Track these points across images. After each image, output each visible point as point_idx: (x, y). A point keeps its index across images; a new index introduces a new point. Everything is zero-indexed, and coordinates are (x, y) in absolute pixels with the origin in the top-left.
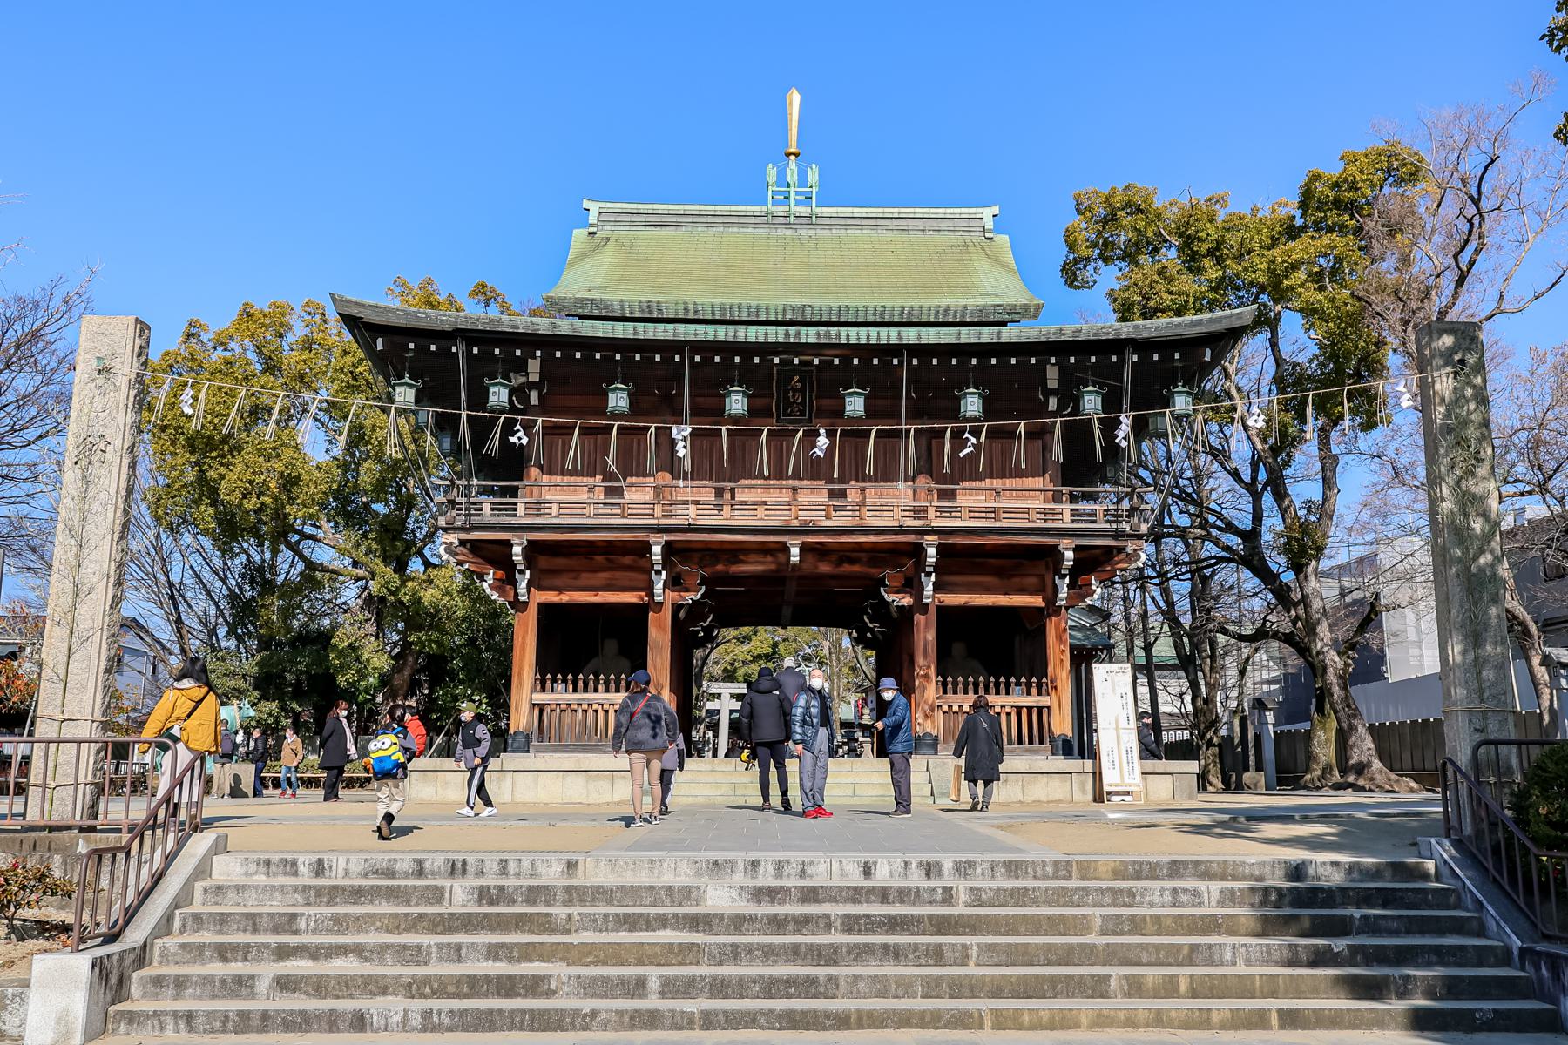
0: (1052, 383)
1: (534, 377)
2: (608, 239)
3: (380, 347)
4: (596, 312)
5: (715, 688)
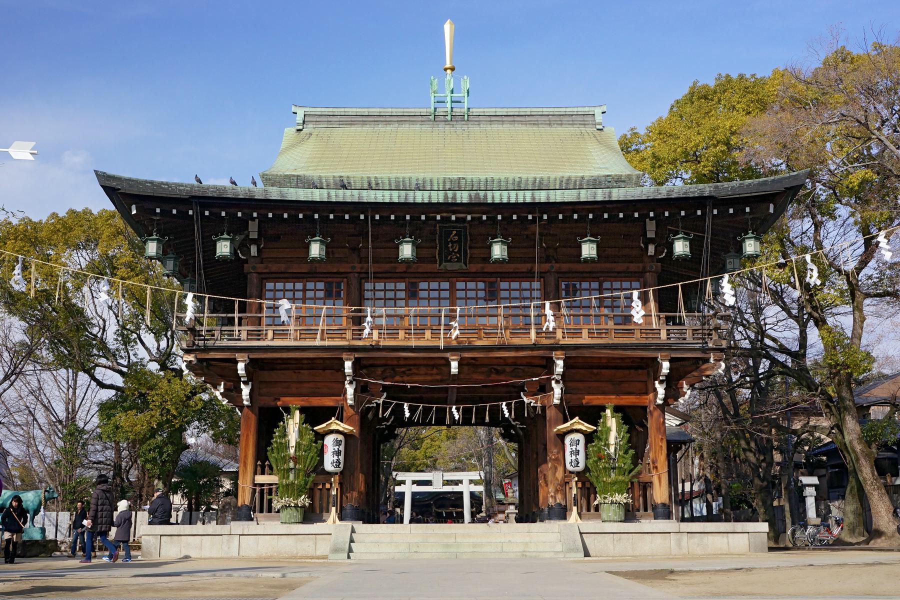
1: (254, 235)
2: (311, 134)
3: (134, 212)
5: (400, 476)
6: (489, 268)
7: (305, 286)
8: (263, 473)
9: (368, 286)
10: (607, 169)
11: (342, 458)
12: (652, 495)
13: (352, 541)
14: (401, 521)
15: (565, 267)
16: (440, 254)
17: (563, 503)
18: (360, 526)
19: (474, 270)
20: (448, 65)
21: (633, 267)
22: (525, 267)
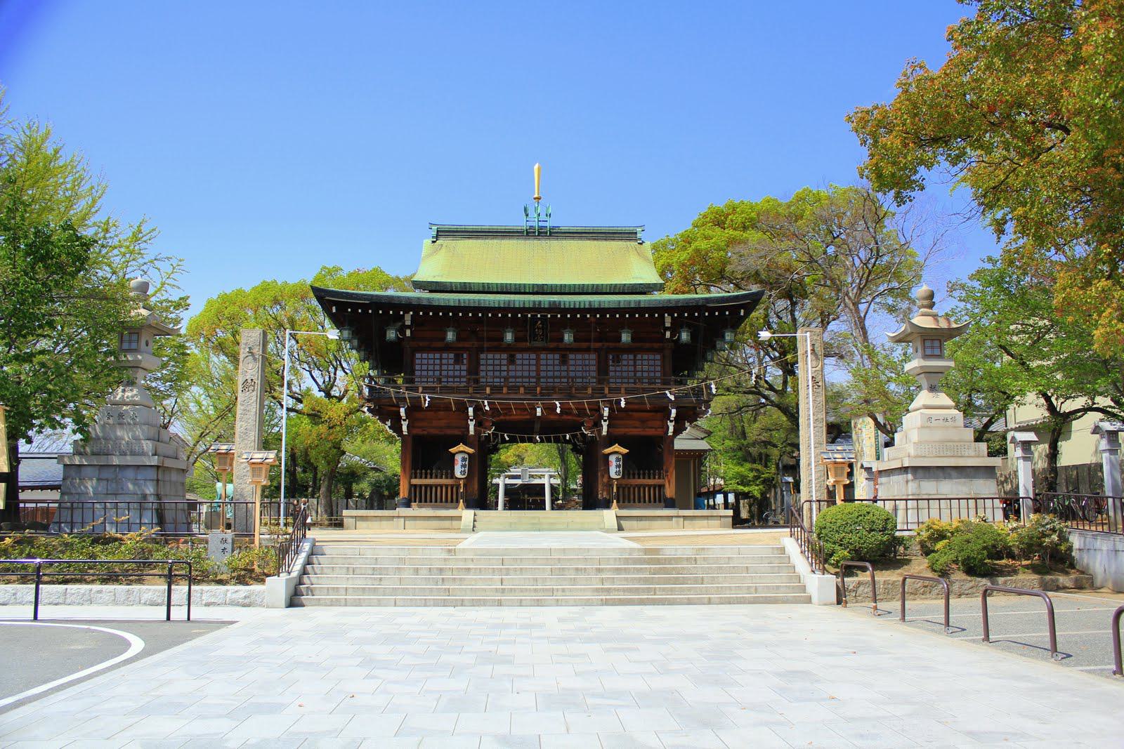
0: (668, 325)
1: (408, 323)
3: (334, 310)
4: (438, 288)
6: (561, 346)
7: (441, 356)
8: (416, 478)
9: (483, 356)
10: (641, 278)
11: (467, 469)
12: (664, 493)
13: (475, 521)
14: (496, 507)
15: (612, 345)
16: (530, 336)
17: (608, 498)
18: (481, 513)
19: (552, 346)
20: (536, 196)
21: (656, 345)
22: (584, 345)
